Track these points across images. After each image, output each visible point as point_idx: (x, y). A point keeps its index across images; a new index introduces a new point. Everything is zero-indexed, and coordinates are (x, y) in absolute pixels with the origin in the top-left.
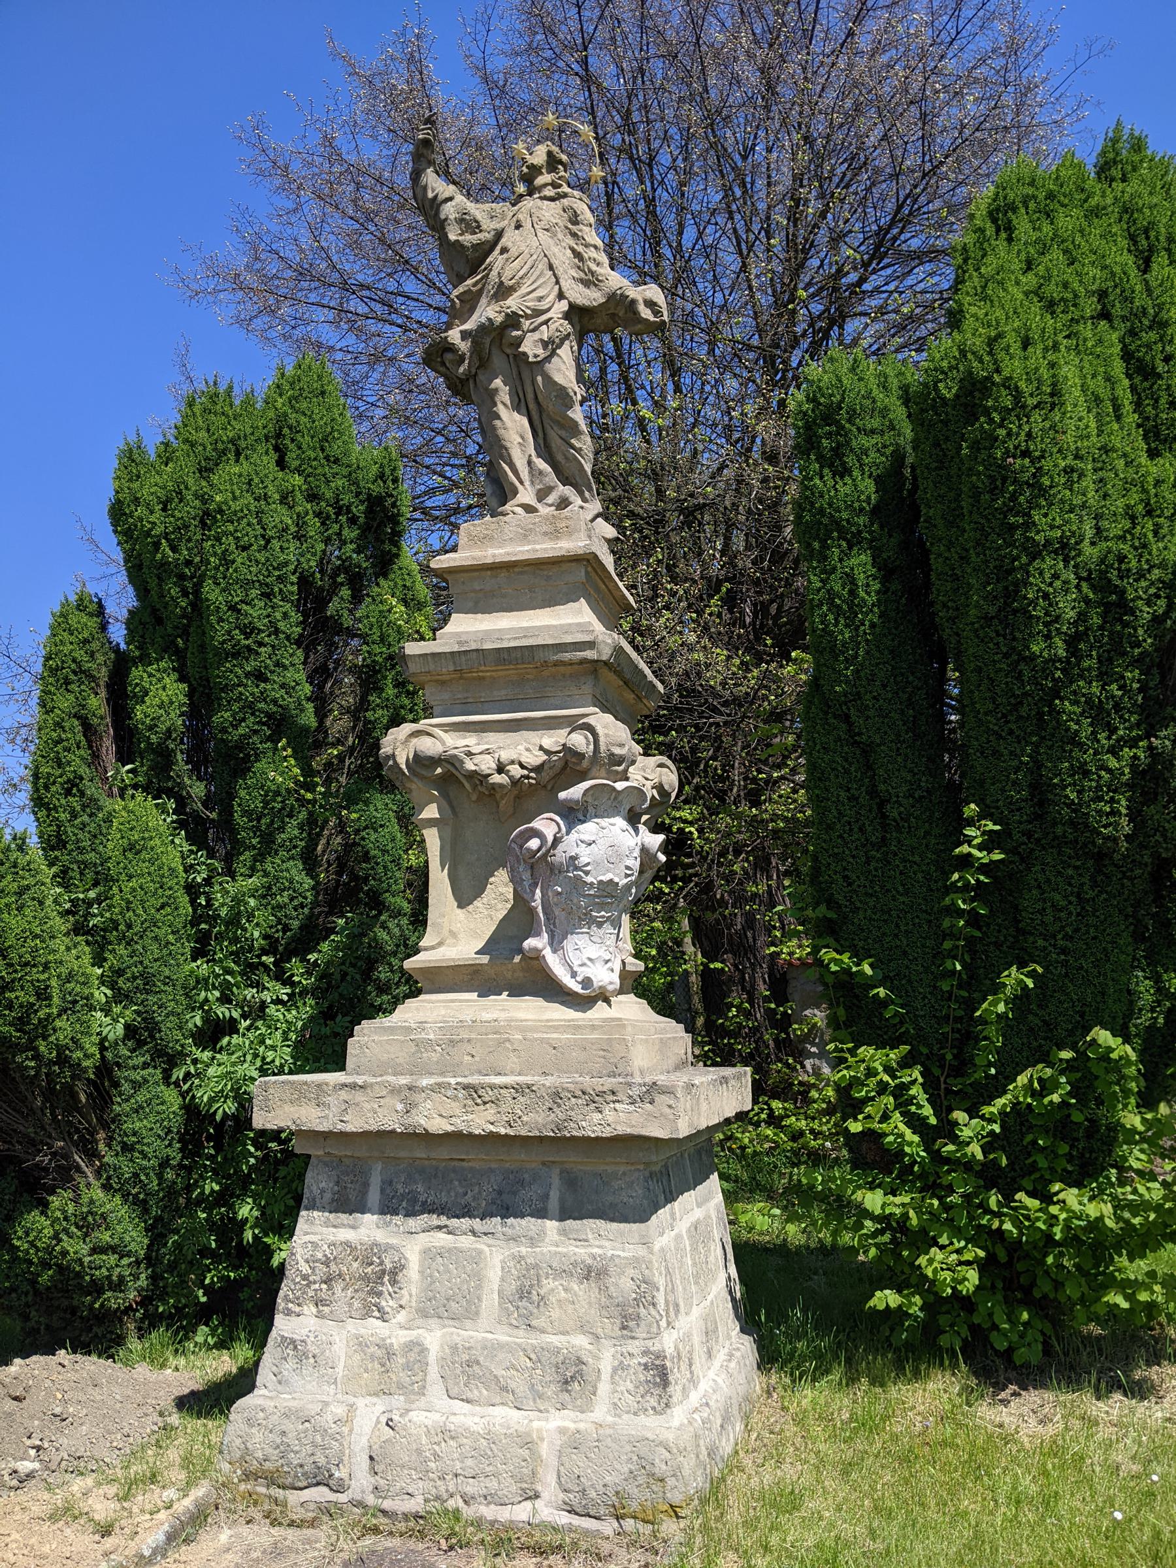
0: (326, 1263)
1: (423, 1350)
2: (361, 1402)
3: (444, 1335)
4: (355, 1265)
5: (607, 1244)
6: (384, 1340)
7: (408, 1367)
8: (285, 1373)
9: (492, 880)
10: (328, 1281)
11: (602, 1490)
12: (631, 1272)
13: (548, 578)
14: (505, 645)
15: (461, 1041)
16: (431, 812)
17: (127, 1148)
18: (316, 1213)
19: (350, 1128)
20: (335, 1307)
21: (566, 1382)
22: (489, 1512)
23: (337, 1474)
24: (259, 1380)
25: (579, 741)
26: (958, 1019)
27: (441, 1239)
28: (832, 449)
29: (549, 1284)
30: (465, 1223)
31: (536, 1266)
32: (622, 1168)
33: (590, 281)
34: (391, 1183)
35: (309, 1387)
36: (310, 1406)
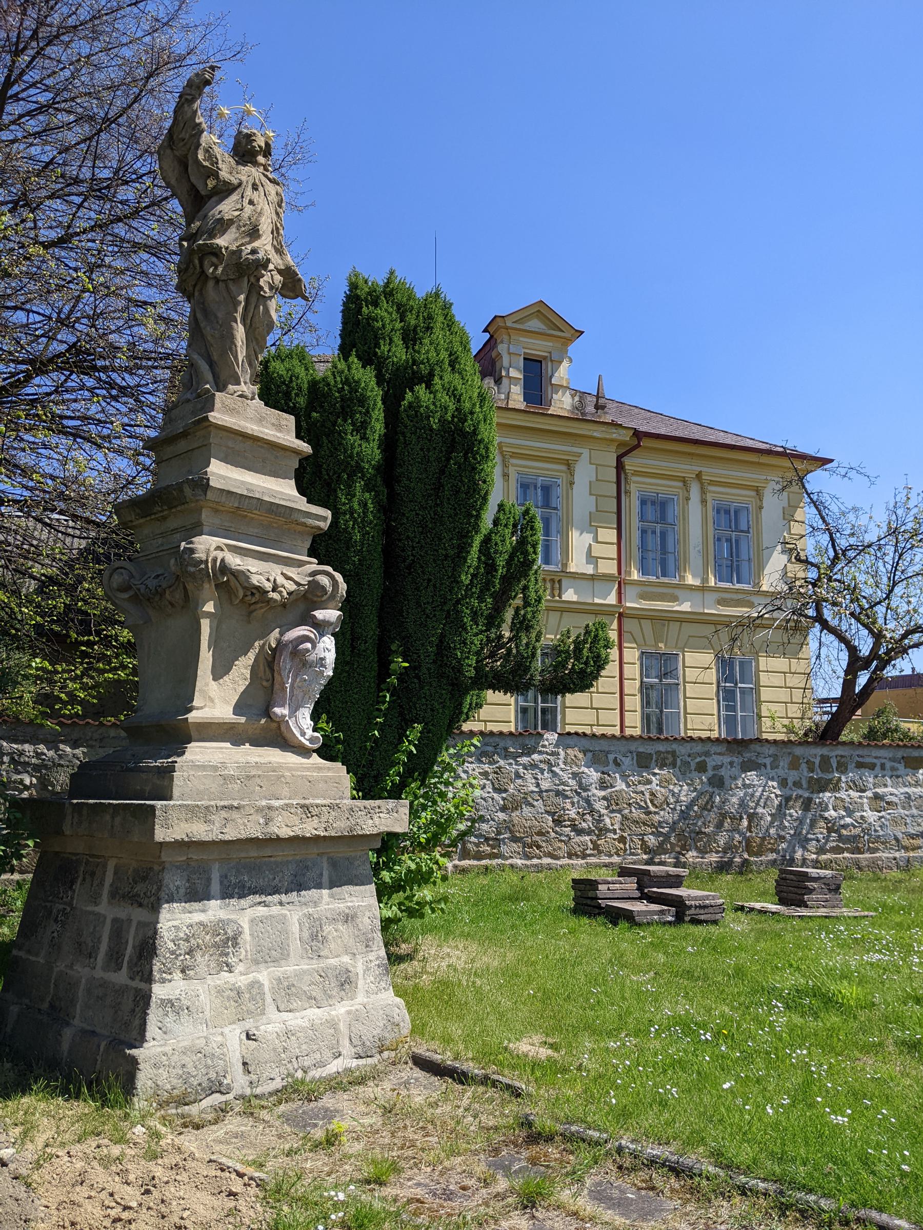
0: (187, 940)
1: (261, 985)
2: (226, 1030)
3: (269, 974)
4: (208, 937)
5: (355, 899)
6: (234, 985)
7: (252, 999)
8: (168, 1025)
9: (236, 663)
10: (190, 952)
11: (372, 1040)
12: (368, 914)
13: (277, 457)
14: (277, 501)
15: (254, 776)
16: (209, 607)
18: (175, 905)
19: (227, 837)
20: (198, 969)
21: (342, 985)
22: (316, 1073)
23: (225, 1082)
24: (148, 1035)
27: (261, 911)
28: (361, 422)
29: (328, 929)
30: (276, 898)
31: (320, 919)
32: (359, 854)
34: (226, 877)
35: (187, 1030)
36: (197, 1042)
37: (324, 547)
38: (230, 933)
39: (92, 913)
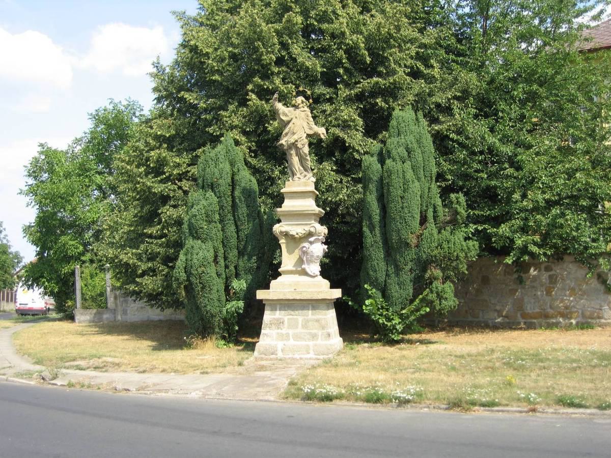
25: (312, 230)
26: (552, 126)
33: (311, 129)
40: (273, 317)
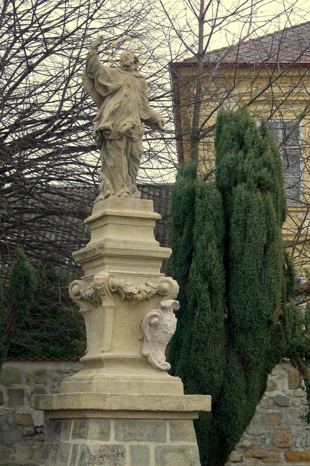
4: (109, 452)
17: (139, 292)
37: (168, 268)
38: (120, 451)
39: (66, 444)
40: (104, 443)
